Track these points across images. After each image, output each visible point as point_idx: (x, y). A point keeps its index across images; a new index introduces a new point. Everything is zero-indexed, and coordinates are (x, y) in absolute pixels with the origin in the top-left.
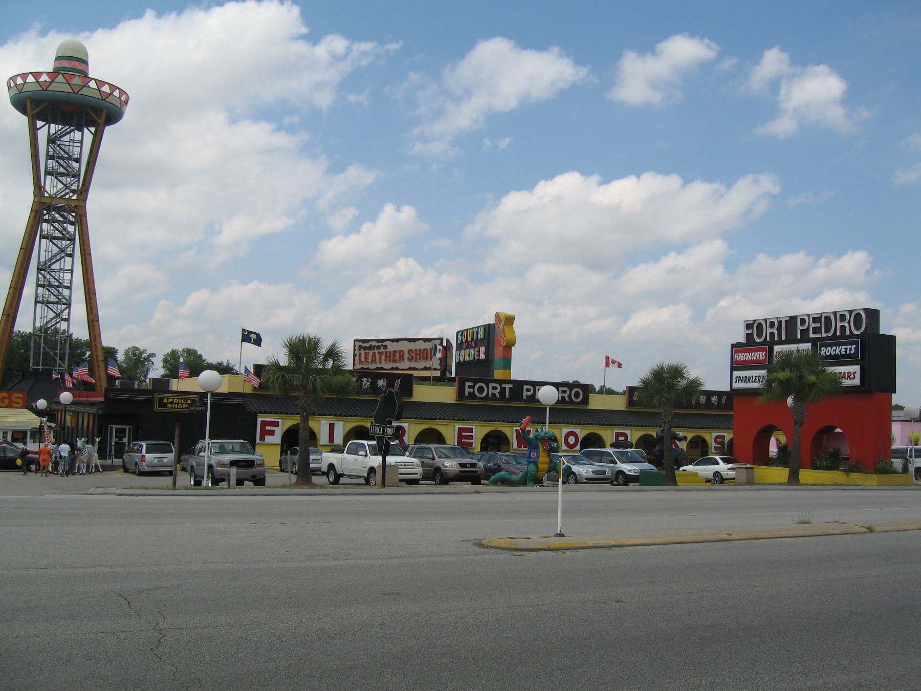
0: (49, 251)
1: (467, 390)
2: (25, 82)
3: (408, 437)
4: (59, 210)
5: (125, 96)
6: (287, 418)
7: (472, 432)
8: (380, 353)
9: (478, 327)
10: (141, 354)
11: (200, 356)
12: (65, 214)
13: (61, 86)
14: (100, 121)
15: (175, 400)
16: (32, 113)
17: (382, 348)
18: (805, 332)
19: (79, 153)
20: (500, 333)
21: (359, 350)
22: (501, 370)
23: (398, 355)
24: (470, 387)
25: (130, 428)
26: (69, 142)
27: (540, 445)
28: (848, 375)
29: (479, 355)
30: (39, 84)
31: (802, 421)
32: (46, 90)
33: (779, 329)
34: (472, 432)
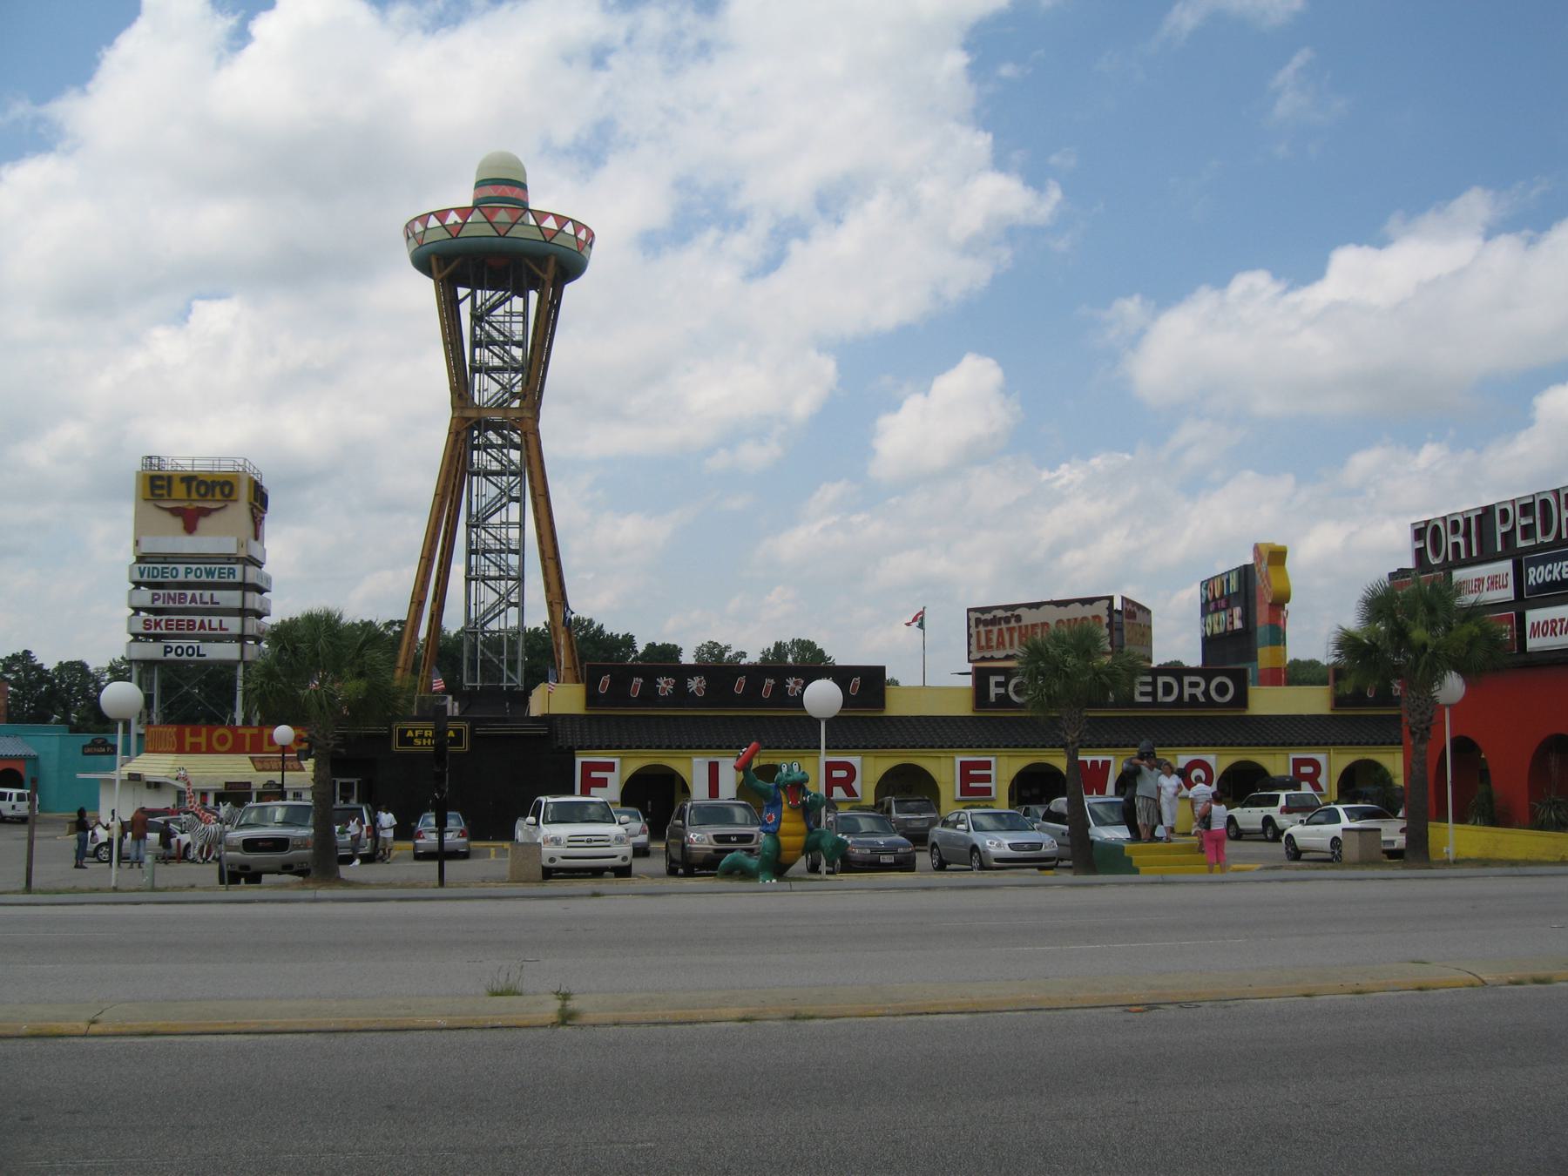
0: (482, 496)
1: (994, 691)
2: (426, 228)
3: (862, 782)
4: (497, 428)
5: (584, 231)
6: (628, 755)
7: (990, 769)
8: (1011, 630)
9: (1228, 573)
10: (722, 653)
11: (821, 652)
12: (505, 432)
13: (478, 228)
14: (545, 277)
15: (426, 732)
16: (441, 276)
17: (1013, 620)
18: (1508, 537)
19: (521, 333)
20: (1263, 581)
21: (977, 626)
22: (1269, 648)
23: (1039, 631)
24: (998, 684)
25: (359, 782)
26: (504, 316)
27: (784, 799)
28: (1552, 625)
29: (1232, 623)
30: (492, 226)
31: (1427, 729)
32: (457, 237)
33: (1467, 535)
34: (990, 769)
